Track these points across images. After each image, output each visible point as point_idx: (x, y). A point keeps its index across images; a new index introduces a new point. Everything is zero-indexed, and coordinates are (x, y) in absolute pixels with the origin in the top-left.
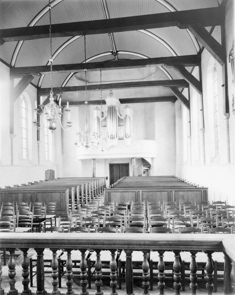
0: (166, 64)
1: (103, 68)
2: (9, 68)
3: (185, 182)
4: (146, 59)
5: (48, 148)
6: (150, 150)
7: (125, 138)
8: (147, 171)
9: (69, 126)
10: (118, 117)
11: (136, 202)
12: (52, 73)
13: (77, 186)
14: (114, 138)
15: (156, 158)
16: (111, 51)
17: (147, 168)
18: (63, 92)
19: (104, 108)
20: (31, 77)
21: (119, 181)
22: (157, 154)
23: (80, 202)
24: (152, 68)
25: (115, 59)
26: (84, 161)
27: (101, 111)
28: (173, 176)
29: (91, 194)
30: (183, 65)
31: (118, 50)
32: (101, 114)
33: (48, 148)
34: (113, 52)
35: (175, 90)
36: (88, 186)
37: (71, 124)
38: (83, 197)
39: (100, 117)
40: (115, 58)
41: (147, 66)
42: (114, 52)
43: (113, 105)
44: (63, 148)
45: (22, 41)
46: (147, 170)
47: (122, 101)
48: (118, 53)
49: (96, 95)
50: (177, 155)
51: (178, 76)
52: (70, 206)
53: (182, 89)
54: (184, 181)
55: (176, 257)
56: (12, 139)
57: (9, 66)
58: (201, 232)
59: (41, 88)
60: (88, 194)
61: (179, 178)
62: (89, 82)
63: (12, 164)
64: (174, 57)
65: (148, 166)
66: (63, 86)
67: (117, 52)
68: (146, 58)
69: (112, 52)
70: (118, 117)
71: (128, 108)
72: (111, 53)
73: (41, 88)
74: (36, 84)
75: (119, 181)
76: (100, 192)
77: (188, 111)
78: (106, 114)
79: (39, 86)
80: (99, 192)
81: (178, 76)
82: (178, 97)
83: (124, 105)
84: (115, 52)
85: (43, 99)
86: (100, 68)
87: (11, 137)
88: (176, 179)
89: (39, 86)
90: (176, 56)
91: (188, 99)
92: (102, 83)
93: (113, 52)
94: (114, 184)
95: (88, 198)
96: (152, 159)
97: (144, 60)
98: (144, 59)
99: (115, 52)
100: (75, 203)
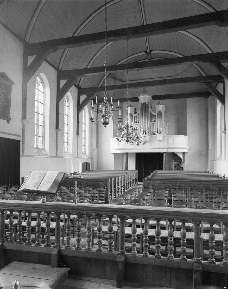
0: (202, 61)
1: (140, 67)
2: (57, 71)
3: (219, 177)
4: (181, 57)
5: (85, 143)
6: (181, 144)
7: (157, 133)
8: (177, 165)
9: (120, 122)
10: (151, 113)
11: (87, 193)
12: (106, 72)
13: (113, 178)
14: (147, 134)
15: (187, 153)
16: (145, 50)
17: (178, 163)
18: (100, 91)
19: (138, 105)
20: (75, 78)
21: (152, 174)
22: (189, 149)
23: (117, 192)
24: (184, 66)
25: (148, 58)
26: (116, 155)
27: (134, 108)
28: (205, 171)
29: (126, 185)
30: (219, 62)
31: (151, 49)
32: (134, 110)
33: (85, 143)
34: (147, 52)
35: (209, 85)
36: (124, 178)
37: (121, 120)
38: (117, 189)
39: (133, 114)
40: (149, 57)
41: (183, 63)
42: (148, 52)
43: (146, 102)
44: (97, 142)
45: (68, 49)
46: (178, 164)
47: (154, 98)
48: (152, 52)
49: (129, 93)
50: (210, 150)
51: (214, 71)
52: (110, 195)
53: (216, 84)
54: (218, 176)
55: (167, 251)
56: (57, 133)
57: (57, 69)
58: (203, 230)
59: (81, 88)
60: (124, 185)
61: (213, 173)
62: (123, 81)
63: (56, 155)
64: (208, 54)
65: (179, 161)
66: (99, 86)
67: (151, 51)
68: (181, 56)
69: (146, 52)
70: (151, 113)
71: (161, 104)
72: (145, 53)
73: (81, 88)
74: (77, 85)
75: (152, 174)
76: (133, 184)
77: (223, 106)
78: (139, 111)
79: (80, 86)
80: (132, 184)
81: (214, 71)
82: (212, 93)
83: (157, 101)
84: (149, 52)
85: (83, 98)
86: (137, 68)
87: (56, 132)
88: (206, 174)
89: (80, 86)
90: (215, 11)
91: (223, 94)
92: (140, 81)
93: (147, 52)
94: (149, 176)
95: (124, 189)
96: (184, 153)
97: (179, 58)
98: (179, 58)
99: (149, 52)
100: (115, 193)
